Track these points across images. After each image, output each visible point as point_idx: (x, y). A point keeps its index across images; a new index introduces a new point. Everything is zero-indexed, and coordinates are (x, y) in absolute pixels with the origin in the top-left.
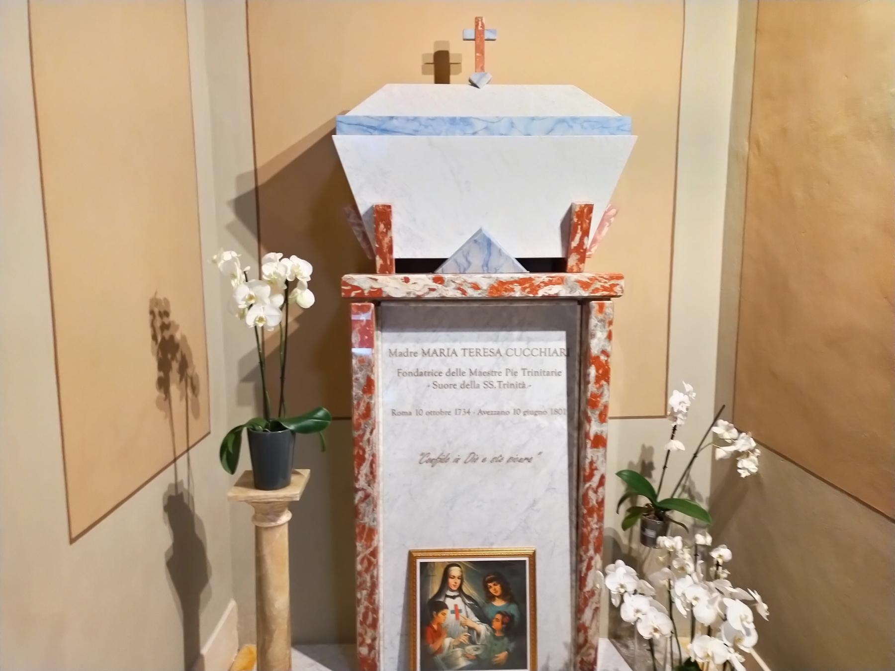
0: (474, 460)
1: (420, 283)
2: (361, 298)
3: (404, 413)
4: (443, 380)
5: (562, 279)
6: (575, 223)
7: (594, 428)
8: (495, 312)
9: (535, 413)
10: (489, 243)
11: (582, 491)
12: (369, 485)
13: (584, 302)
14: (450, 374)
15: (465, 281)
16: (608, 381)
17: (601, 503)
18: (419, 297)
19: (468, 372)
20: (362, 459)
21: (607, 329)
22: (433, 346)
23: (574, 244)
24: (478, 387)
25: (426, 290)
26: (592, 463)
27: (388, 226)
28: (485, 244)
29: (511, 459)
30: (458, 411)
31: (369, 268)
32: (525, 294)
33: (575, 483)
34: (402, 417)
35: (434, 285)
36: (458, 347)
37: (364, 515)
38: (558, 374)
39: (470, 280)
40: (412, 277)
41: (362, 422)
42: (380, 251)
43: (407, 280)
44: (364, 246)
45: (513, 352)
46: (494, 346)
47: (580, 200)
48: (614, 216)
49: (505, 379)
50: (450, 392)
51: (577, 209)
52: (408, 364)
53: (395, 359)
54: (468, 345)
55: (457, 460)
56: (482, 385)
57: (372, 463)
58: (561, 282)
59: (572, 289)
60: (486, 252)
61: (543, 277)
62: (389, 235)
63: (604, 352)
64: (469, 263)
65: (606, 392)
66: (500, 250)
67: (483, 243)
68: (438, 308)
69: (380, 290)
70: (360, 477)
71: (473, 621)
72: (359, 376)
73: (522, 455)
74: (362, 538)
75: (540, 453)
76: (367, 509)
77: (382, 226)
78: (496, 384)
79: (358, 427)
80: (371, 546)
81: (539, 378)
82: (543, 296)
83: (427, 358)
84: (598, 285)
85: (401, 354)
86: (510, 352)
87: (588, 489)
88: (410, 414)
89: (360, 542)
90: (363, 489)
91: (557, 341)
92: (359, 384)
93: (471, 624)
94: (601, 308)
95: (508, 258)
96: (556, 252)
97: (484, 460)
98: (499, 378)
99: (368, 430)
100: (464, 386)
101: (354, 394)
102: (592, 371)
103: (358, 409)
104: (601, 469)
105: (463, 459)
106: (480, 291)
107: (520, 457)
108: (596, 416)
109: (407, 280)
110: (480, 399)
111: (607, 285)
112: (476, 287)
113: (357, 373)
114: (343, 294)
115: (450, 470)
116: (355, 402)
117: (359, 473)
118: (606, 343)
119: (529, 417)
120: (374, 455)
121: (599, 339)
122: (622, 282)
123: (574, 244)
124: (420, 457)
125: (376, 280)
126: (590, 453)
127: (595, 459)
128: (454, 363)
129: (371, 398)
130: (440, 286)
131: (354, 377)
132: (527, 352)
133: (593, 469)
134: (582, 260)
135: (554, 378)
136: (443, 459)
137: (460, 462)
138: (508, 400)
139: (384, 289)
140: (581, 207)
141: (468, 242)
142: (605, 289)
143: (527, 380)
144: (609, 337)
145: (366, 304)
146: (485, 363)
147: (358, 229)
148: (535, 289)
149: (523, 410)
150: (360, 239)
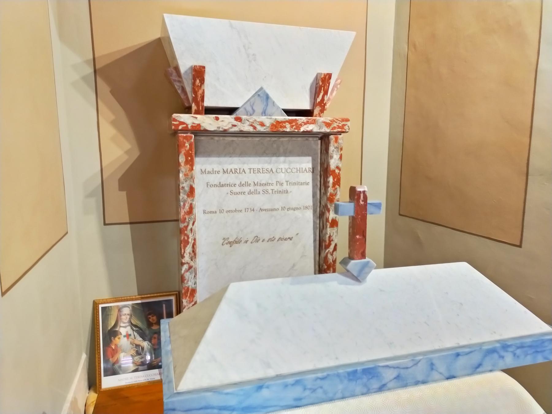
0: (257, 241)
1: (226, 121)
2: (185, 130)
3: (211, 212)
4: (237, 189)
5: (315, 120)
6: (321, 85)
7: (332, 215)
8: (274, 140)
9: (294, 209)
10: (267, 97)
11: (323, 255)
12: (192, 260)
13: (324, 138)
14: (241, 185)
15: (255, 120)
16: (339, 186)
17: (334, 261)
18: (225, 130)
19: (252, 184)
20: (187, 243)
21: (340, 153)
22: (230, 167)
23: (319, 100)
24: (259, 193)
25: (230, 126)
26: (330, 237)
27: (202, 81)
28: (265, 98)
29: (280, 239)
30: (246, 210)
31: (188, 110)
32: (292, 130)
33: (318, 251)
34: (210, 215)
35: (235, 123)
36: (246, 167)
37: (188, 281)
38: (307, 184)
39: (258, 120)
40: (221, 117)
41: (187, 217)
42: (195, 100)
43: (217, 119)
44: (182, 96)
45: (280, 170)
46: (269, 167)
47: (325, 71)
48: (340, 84)
49: (276, 188)
50: (241, 197)
51: (323, 76)
52: (214, 179)
53: (204, 175)
54: (252, 166)
55: (246, 242)
56: (261, 192)
57: (194, 245)
58: (314, 122)
59: (320, 127)
60: (265, 103)
61: (304, 119)
62: (202, 88)
63: (338, 167)
64: (254, 111)
65: (338, 193)
66: (274, 102)
67: (263, 96)
68: (233, 141)
69: (199, 125)
70: (185, 255)
71: (139, 340)
72: (184, 185)
73: (287, 236)
74: (187, 296)
75: (297, 234)
76: (190, 276)
77: (198, 81)
78: (270, 191)
79: (184, 220)
80: (193, 301)
81: (296, 186)
82: (303, 132)
83: (226, 175)
84: (335, 125)
85: (209, 172)
86: (279, 171)
87: (327, 253)
88: (216, 212)
89: (186, 299)
90: (187, 263)
91: (306, 163)
92: (185, 191)
93: (138, 343)
94: (336, 140)
95: (278, 107)
96: (306, 105)
97: (263, 241)
98: (272, 187)
99: (191, 223)
100: (250, 193)
101: (181, 198)
102: (331, 180)
103: (184, 208)
104: (336, 240)
105: (250, 240)
106: (265, 127)
107: (285, 237)
108: (333, 208)
109: (217, 119)
110: (260, 201)
111: (340, 125)
112: (262, 124)
113: (183, 183)
114: (173, 127)
115: (242, 248)
116: (182, 204)
117: (184, 252)
118: (339, 162)
119: (291, 212)
120: (195, 240)
121: (335, 159)
122: (349, 123)
123: (319, 100)
124: (222, 241)
125: (196, 118)
126: (329, 230)
127: (332, 234)
128: (244, 178)
129: (193, 200)
130: (239, 123)
131: (181, 186)
132: (289, 170)
133: (330, 241)
134: (322, 111)
135: (307, 186)
136: (237, 242)
137: (248, 242)
138: (278, 201)
139: (202, 125)
140: (324, 75)
141: (253, 96)
142: (339, 127)
143: (289, 188)
144: (341, 158)
145: (189, 134)
146: (263, 178)
147: (178, 84)
148: (298, 127)
149: (286, 208)
150: (179, 92)
